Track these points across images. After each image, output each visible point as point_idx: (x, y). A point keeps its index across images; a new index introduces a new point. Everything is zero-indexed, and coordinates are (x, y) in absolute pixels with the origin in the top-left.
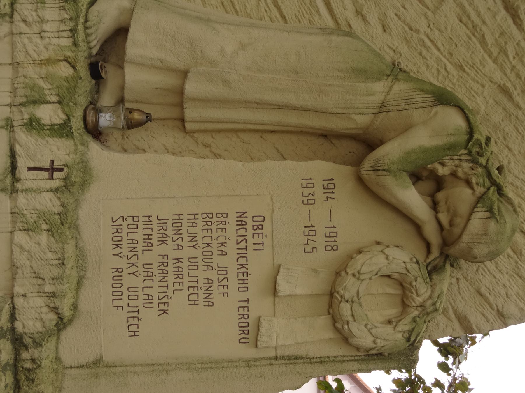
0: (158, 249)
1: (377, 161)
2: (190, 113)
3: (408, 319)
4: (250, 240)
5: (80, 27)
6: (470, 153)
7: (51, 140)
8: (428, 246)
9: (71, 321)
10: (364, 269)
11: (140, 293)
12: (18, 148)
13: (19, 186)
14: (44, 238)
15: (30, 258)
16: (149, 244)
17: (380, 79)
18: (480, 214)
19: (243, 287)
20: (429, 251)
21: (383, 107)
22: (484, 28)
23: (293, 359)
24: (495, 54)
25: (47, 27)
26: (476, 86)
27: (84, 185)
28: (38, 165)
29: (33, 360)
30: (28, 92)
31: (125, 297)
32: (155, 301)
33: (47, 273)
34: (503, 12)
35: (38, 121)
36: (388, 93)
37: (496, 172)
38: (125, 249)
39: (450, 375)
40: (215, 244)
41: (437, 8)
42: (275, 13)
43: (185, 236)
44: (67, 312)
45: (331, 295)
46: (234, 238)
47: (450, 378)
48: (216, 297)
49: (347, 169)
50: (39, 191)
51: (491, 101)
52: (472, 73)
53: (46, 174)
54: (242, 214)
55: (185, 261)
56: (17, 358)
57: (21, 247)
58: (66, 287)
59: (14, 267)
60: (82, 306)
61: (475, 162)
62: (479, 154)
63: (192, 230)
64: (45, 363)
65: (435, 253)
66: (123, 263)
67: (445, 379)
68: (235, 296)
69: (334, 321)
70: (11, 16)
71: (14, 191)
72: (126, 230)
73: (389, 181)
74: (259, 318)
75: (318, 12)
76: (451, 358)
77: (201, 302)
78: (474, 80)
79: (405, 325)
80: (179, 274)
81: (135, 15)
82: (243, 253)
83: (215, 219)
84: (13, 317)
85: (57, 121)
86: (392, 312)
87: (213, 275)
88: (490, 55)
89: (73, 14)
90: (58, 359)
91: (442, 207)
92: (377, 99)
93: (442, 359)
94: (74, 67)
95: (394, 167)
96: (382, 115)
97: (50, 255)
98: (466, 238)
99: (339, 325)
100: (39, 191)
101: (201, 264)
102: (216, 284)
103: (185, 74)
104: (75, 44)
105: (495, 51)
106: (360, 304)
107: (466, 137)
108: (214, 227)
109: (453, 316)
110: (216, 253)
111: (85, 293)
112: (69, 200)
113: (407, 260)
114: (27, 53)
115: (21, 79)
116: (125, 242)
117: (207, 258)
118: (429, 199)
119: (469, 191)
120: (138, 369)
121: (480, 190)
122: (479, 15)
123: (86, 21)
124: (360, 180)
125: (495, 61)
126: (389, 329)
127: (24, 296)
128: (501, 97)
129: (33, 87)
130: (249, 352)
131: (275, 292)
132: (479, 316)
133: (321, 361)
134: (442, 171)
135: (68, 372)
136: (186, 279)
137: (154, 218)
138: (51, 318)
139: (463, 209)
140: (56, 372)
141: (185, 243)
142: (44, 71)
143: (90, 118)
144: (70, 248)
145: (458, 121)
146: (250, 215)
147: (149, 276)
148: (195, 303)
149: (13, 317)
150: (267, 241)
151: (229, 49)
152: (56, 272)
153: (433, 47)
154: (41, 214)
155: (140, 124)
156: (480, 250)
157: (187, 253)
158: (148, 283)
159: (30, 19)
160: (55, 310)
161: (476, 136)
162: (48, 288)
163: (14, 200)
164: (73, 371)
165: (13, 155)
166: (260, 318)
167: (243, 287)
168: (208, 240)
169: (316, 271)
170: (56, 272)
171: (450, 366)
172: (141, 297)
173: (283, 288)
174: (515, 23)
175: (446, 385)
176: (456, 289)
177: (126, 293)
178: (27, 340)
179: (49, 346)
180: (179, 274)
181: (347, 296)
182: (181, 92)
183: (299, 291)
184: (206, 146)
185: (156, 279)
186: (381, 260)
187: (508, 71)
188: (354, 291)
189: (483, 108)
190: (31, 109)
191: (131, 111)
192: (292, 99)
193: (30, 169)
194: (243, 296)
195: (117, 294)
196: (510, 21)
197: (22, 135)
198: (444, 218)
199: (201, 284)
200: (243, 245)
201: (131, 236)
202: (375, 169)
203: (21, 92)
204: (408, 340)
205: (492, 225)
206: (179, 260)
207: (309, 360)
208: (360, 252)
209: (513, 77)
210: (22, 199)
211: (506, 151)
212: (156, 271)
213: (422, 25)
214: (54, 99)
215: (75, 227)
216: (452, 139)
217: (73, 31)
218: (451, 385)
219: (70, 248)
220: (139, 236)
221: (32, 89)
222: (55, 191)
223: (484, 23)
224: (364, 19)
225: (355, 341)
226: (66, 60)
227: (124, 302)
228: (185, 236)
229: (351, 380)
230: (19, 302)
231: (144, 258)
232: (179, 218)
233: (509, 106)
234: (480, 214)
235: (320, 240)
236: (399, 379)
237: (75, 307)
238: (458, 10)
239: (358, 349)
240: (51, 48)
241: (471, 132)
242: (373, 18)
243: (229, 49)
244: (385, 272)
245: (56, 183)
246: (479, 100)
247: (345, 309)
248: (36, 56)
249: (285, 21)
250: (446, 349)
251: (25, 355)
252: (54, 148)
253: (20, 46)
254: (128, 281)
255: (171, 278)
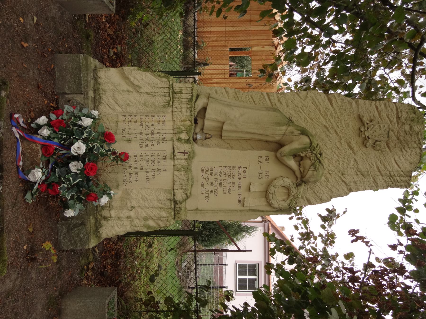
0: (215, 177)
1: (282, 152)
2: (224, 134)
3: (289, 199)
4: (242, 175)
5: (193, 110)
6: (311, 150)
7: (184, 144)
8: (297, 178)
9: (189, 197)
10: (277, 184)
11: (209, 190)
12: (175, 147)
13: (175, 157)
14: (183, 173)
15: (179, 178)
16: (212, 175)
17: (284, 126)
18: (312, 169)
19: (240, 189)
20: (297, 180)
22: (320, 107)
23: (254, 210)
24: (324, 115)
25: (183, 110)
26: (317, 126)
27: (193, 157)
28: (181, 152)
29: (180, 208)
30: (178, 130)
31: (205, 191)
32: (214, 192)
33: (183, 183)
34: (327, 101)
35: (181, 138)
36: (286, 130)
37: (319, 156)
38: (205, 177)
39: (326, 230)
40: (231, 176)
41: (305, 99)
42: (251, 100)
43: (223, 173)
44: (189, 194)
45: (266, 192)
46: (237, 174)
47: (326, 232)
48: (232, 191)
49: (273, 153)
50: (181, 159)
51: (322, 130)
52: (316, 121)
53: (183, 154)
54: (240, 167)
55: (222, 180)
56: (175, 207)
57: (176, 176)
58: (189, 187)
59: (174, 181)
60: (192, 193)
61: (312, 153)
62: (314, 150)
63: (225, 171)
64: (183, 209)
65: (299, 180)
66: (204, 181)
67: (324, 233)
68: (237, 191)
69: (267, 199)
70: (172, 106)
71: (174, 159)
72: (205, 171)
73: (285, 158)
74: (244, 198)
75: (265, 100)
76: (327, 223)
77: (227, 193)
78: (316, 124)
79: (288, 201)
80: (221, 184)
81: (208, 105)
82: (240, 178)
83: (232, 168)
84: (174, 196)
85: (186, 139)
86: (285, 197)
87: (231, 185)
88: (322, 115)
89: (191, 106)
90: (185, 208)
91: (302, 166)
92: (283, 132)
93: (323, 223)
94: (191, 122)
95: (286, 154)
96: (284, 137)
97: (184, 178)
98: (307, 176)
99: (268, 201)
100: (181, 159)
101: (227, 181)
102: (232, 187)
103: (223, 123)
104: (191, 115)
105: (324, 114)
106: (275, 195)
107: (309, 145)
108: (231, 170)
109: (305, 199)
110: (232, 178)
111: (193, 189)
112: (189, 162)
113: (290, 182)
114: (177, 118)
115: (176, 126)
116: (205, 174)
117: (229, 180)
118: (298, 163)
119: (310, 161)
120: (208, 211)
121: (313, 161)
122: (319, 102)
123: (194, 107)
124: (276, 157)
125: (323, 117)
126: (284, 202)
127: (177, 189)
128: (325, 129)
129: (179, 128)
130: (241, 208)
131: (249, 190)
132: (314, 200)
133: (263, 211)
134: (302, 155)
135: (188, 212)
136: (223, 186)
137: (213, 168)
138: (185, 196)
139: (307, 167)
140: (185, 211)
141: (223, 175)
142: (182, 123)
143: (195, 137)
144: (190, 176)
145: (308, 140)
146: (242, 167)
147: (212, 184)
148: (225, 193)
149: (174, 196)
150: (247, 175)
151: (237, 116)
152: (186, 183)
153: (303, 113)
154: (182, 166)
155: (209, 138)
156: (311, 180)
157: (223, 178)
158: (212, 187)
159: (178, 107)
160: (186, 194)
161: (313, 145)
162: (184, 187)
163: (174, 162)
164: (190, 211)
165: (173, 148)
166: (244, 198)
167: (240, 189)
168: (229, 174)
169: (262, 184)
170: (186, 183)
171: (326, 226)
172: (210, 191)
173: (252, 189)
174: (331, 105)
175: (324, 235)
176: (307, 191)
177: (205, 189)
178: (178, 202)
179: (184, 204)
180: (221, 184)
181: (271, 192)
182: (222, 128)
183: (257, 190)
184: (228, 144)
185: (214, 186)
186: (282, 182)
187: (328, 121)
188: (273, 191)
189: (319, 133)
190: (179, 135)
191: (206, 134)
192: (256, 131)
193: (178, 153)
194: (240, 191)
195: (202, 190)
196: (329, 104)
197: (176, 143)
198: (302, 169)
199: (227, 187)
200: (240, 176)
201: (207, 173)
202: (281, 154)
203: (176, 130)
204: (289, 206)
205: (315, 172)
206: (221, 180)
207: (259, 211)
208: (276, 179)
209: (329, 123)
210: (176, 162)
211: (325, 147)
212: (214, 183)
213: (300, 105)
214: (185, 132)
215: (191, 170)
216: (305, 146)
217: (191, 111)
218: (326, 235)
219: (190, 176)
220: (209, 173)
221: (179, 129)
222: (186, 159)
223: (320, 105)
224: (281, 103)
225: (273, 206)
226: (189, 120)
227: (205, 192)
228: (223, 173)
229: (276, 227)
230: (176, 191)
231: (211, 179)
233: (327, 132)
234: (312, 169)
235: (264, 175)
236: (302, 233)
237: (190, 193)
238: (312, 100)
239: (274, 208)
240: (184, 116)
241: (311, 143)
242: (284, 103)
243: (237, 116)
244: (283, 185)
245: (186, 157)
246: (318, 130)
247: (270, 196)
248: (180, 119)
249: (255, 104)
250: (324, 218)
251: (177, 206)
252: (185, 147)
253: (175, 115)
254: (206, 186)
255: (218, 185)
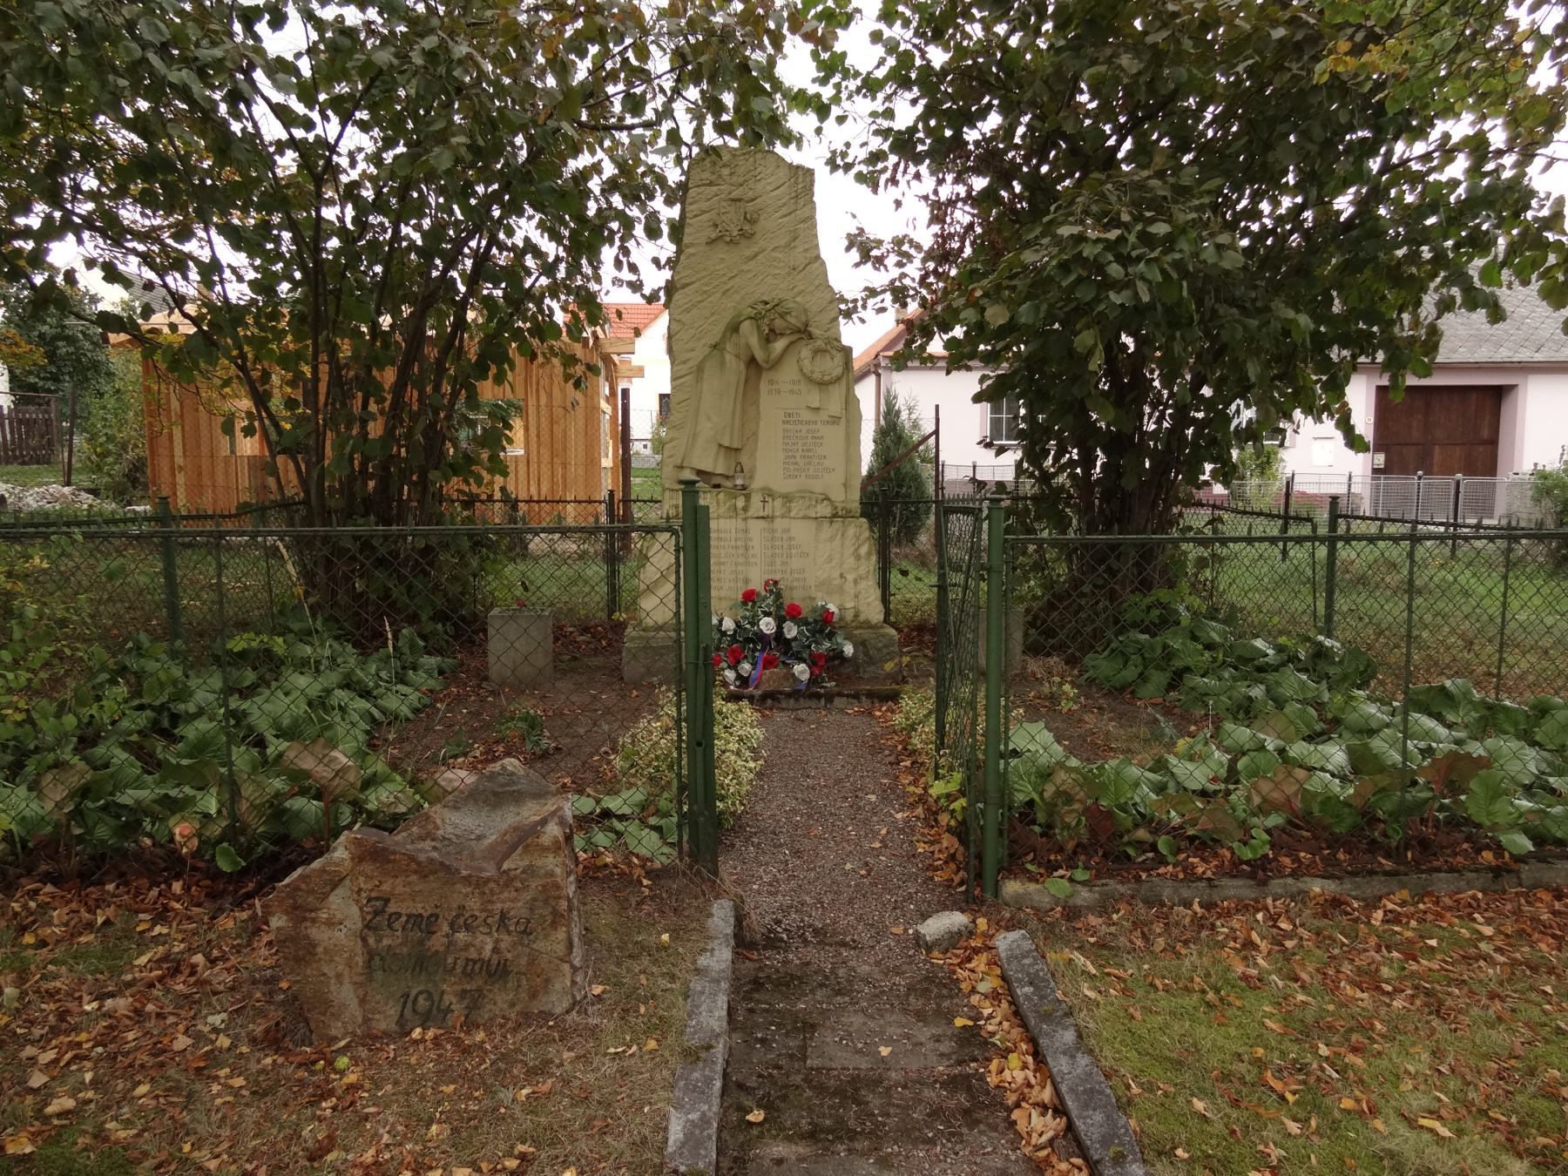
2: (735, 446)
18: (789, 318)
19: (815, 423)
21: (737, 356)
49: (765, 375)
68: (819, 426)
79: (834, 352)
82: (801, 422)
156: (803, 319)
167: (815, 423)
173: (816, 405)
178: (1147, 56)
195: (816, 477)
197: (749, 514)
232: (1381, 528)
234: (789, 318)
242: (688, 355)
247: (826, 378)
